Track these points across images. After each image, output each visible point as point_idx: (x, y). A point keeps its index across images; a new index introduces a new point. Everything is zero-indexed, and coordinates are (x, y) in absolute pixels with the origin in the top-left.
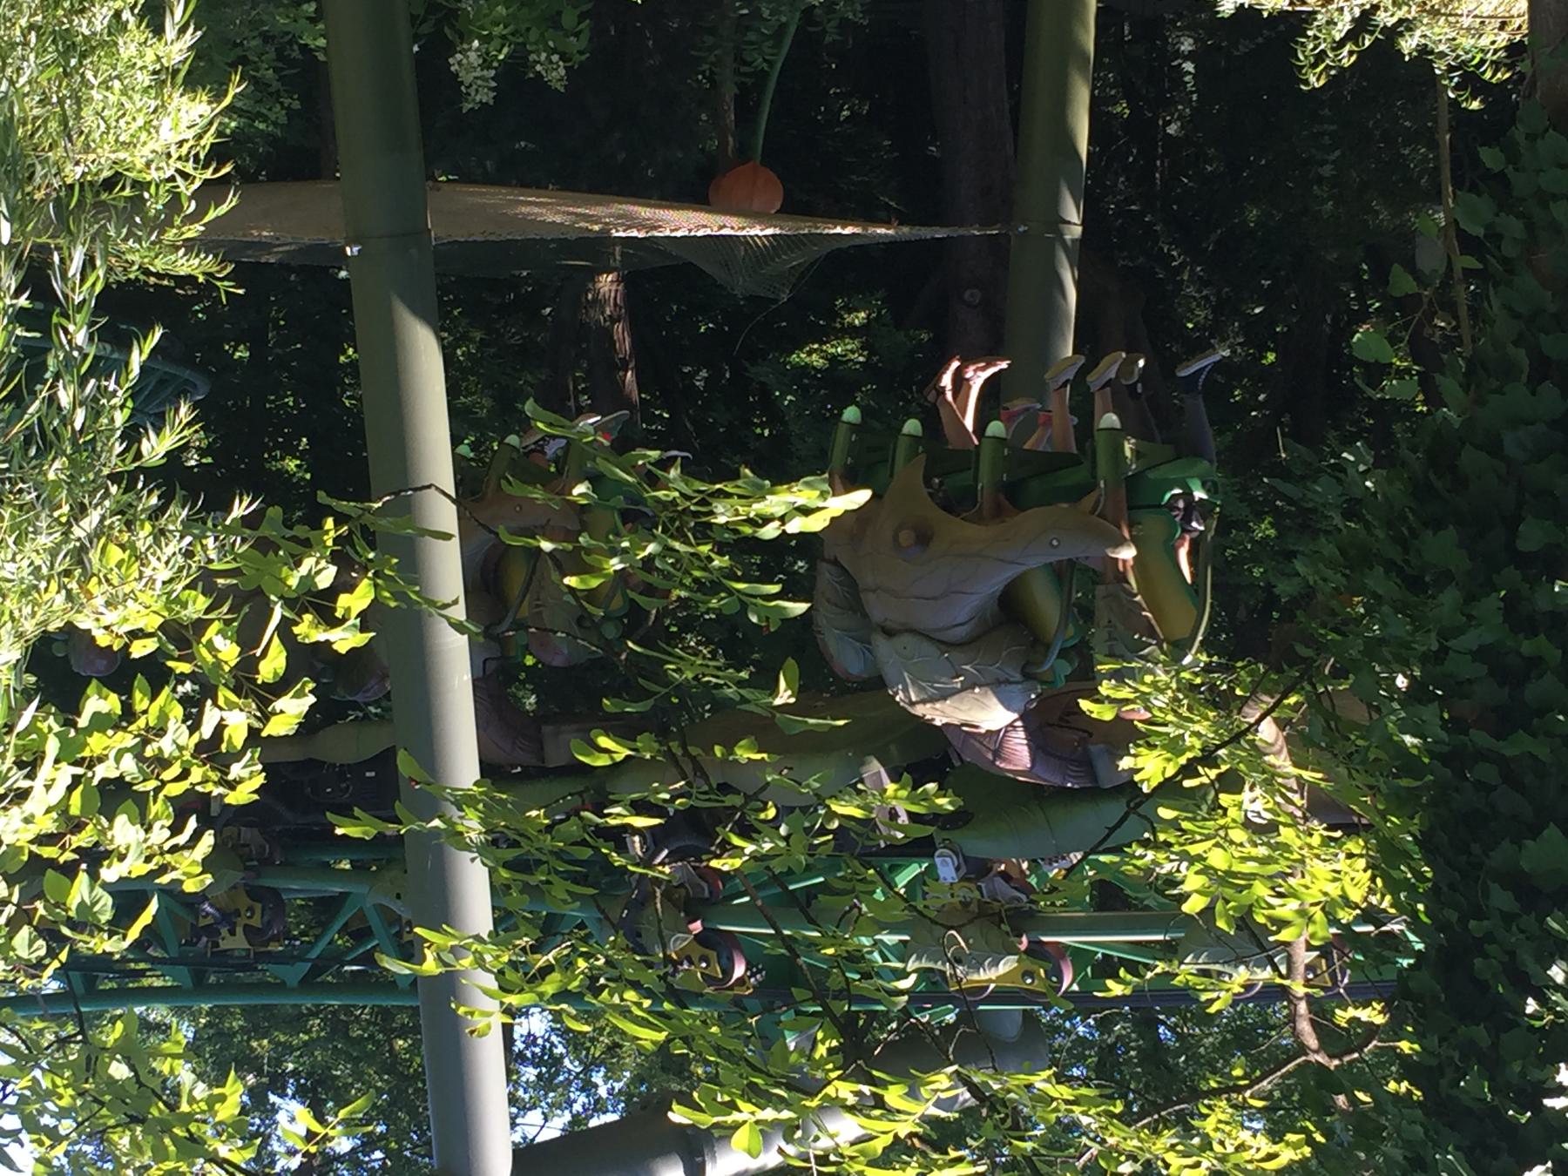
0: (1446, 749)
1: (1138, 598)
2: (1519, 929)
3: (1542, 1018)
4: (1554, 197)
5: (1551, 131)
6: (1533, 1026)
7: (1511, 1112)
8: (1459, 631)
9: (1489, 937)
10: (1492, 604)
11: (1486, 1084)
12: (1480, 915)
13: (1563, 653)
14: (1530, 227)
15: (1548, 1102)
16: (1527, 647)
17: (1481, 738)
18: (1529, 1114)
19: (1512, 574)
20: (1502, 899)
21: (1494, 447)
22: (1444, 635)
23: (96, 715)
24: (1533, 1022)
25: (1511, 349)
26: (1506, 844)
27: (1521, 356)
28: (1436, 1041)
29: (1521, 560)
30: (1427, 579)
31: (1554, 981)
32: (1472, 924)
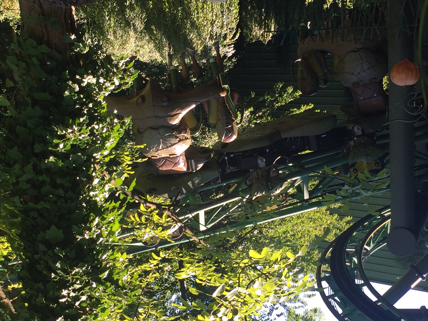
0: (23, 209)
1: (81, 197)
2: (47, 255)
3: (56, 278)
4: (33, 56)
5: (29, 38)
6: (54, 281)
7: (51, 305)
8: (20, 176)
9: (40, 259)
10: (29, 167)
11: (44, 299)
12: (37, 253)
13: (51, 180)
14: (27, 64)
15: (61, 300)
16: (40, 178)
17: (31, 205)
18: (56, 305)
19: (34, 159)
20: (42, 247)
21: (25, 125)
22: (17, 177)
23: (154, 299)
24: (54, 280)
25: (26, 98)
26: (41, 233)
27: (29, 100)
28: (29, 289)
29: (36, 155)
30: (11, 163)
31: (58, 267)
32: (35, 256)
